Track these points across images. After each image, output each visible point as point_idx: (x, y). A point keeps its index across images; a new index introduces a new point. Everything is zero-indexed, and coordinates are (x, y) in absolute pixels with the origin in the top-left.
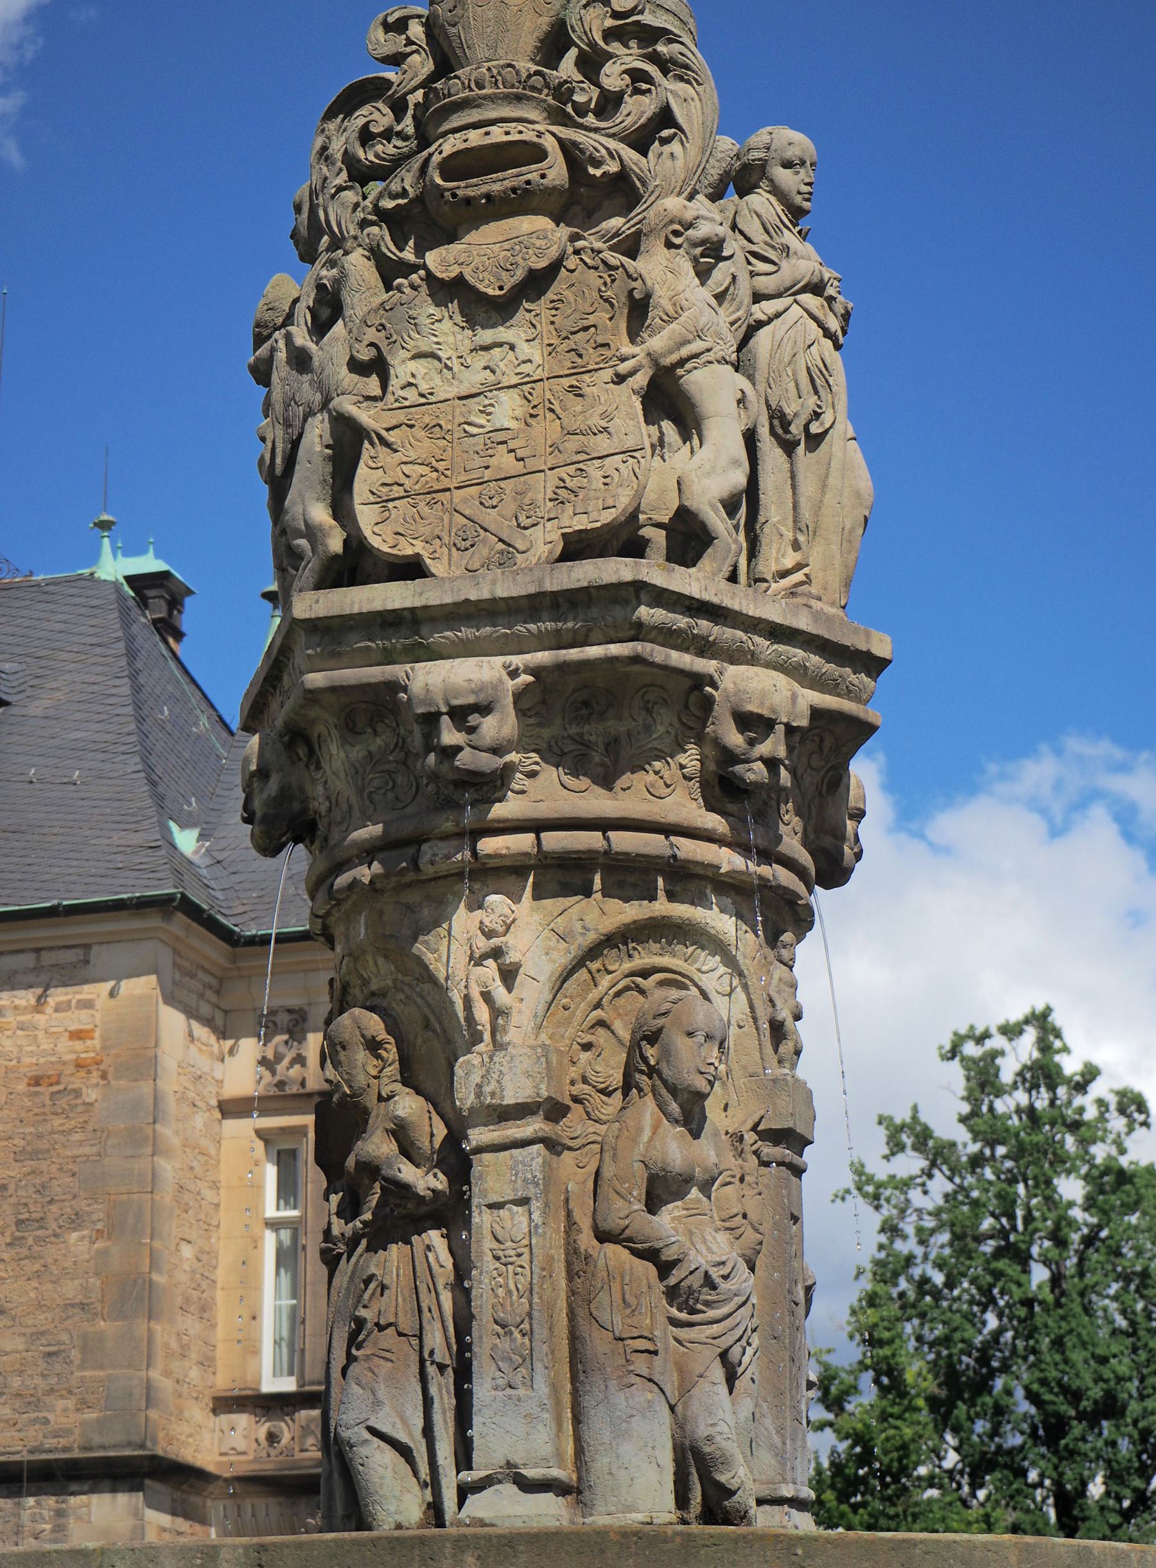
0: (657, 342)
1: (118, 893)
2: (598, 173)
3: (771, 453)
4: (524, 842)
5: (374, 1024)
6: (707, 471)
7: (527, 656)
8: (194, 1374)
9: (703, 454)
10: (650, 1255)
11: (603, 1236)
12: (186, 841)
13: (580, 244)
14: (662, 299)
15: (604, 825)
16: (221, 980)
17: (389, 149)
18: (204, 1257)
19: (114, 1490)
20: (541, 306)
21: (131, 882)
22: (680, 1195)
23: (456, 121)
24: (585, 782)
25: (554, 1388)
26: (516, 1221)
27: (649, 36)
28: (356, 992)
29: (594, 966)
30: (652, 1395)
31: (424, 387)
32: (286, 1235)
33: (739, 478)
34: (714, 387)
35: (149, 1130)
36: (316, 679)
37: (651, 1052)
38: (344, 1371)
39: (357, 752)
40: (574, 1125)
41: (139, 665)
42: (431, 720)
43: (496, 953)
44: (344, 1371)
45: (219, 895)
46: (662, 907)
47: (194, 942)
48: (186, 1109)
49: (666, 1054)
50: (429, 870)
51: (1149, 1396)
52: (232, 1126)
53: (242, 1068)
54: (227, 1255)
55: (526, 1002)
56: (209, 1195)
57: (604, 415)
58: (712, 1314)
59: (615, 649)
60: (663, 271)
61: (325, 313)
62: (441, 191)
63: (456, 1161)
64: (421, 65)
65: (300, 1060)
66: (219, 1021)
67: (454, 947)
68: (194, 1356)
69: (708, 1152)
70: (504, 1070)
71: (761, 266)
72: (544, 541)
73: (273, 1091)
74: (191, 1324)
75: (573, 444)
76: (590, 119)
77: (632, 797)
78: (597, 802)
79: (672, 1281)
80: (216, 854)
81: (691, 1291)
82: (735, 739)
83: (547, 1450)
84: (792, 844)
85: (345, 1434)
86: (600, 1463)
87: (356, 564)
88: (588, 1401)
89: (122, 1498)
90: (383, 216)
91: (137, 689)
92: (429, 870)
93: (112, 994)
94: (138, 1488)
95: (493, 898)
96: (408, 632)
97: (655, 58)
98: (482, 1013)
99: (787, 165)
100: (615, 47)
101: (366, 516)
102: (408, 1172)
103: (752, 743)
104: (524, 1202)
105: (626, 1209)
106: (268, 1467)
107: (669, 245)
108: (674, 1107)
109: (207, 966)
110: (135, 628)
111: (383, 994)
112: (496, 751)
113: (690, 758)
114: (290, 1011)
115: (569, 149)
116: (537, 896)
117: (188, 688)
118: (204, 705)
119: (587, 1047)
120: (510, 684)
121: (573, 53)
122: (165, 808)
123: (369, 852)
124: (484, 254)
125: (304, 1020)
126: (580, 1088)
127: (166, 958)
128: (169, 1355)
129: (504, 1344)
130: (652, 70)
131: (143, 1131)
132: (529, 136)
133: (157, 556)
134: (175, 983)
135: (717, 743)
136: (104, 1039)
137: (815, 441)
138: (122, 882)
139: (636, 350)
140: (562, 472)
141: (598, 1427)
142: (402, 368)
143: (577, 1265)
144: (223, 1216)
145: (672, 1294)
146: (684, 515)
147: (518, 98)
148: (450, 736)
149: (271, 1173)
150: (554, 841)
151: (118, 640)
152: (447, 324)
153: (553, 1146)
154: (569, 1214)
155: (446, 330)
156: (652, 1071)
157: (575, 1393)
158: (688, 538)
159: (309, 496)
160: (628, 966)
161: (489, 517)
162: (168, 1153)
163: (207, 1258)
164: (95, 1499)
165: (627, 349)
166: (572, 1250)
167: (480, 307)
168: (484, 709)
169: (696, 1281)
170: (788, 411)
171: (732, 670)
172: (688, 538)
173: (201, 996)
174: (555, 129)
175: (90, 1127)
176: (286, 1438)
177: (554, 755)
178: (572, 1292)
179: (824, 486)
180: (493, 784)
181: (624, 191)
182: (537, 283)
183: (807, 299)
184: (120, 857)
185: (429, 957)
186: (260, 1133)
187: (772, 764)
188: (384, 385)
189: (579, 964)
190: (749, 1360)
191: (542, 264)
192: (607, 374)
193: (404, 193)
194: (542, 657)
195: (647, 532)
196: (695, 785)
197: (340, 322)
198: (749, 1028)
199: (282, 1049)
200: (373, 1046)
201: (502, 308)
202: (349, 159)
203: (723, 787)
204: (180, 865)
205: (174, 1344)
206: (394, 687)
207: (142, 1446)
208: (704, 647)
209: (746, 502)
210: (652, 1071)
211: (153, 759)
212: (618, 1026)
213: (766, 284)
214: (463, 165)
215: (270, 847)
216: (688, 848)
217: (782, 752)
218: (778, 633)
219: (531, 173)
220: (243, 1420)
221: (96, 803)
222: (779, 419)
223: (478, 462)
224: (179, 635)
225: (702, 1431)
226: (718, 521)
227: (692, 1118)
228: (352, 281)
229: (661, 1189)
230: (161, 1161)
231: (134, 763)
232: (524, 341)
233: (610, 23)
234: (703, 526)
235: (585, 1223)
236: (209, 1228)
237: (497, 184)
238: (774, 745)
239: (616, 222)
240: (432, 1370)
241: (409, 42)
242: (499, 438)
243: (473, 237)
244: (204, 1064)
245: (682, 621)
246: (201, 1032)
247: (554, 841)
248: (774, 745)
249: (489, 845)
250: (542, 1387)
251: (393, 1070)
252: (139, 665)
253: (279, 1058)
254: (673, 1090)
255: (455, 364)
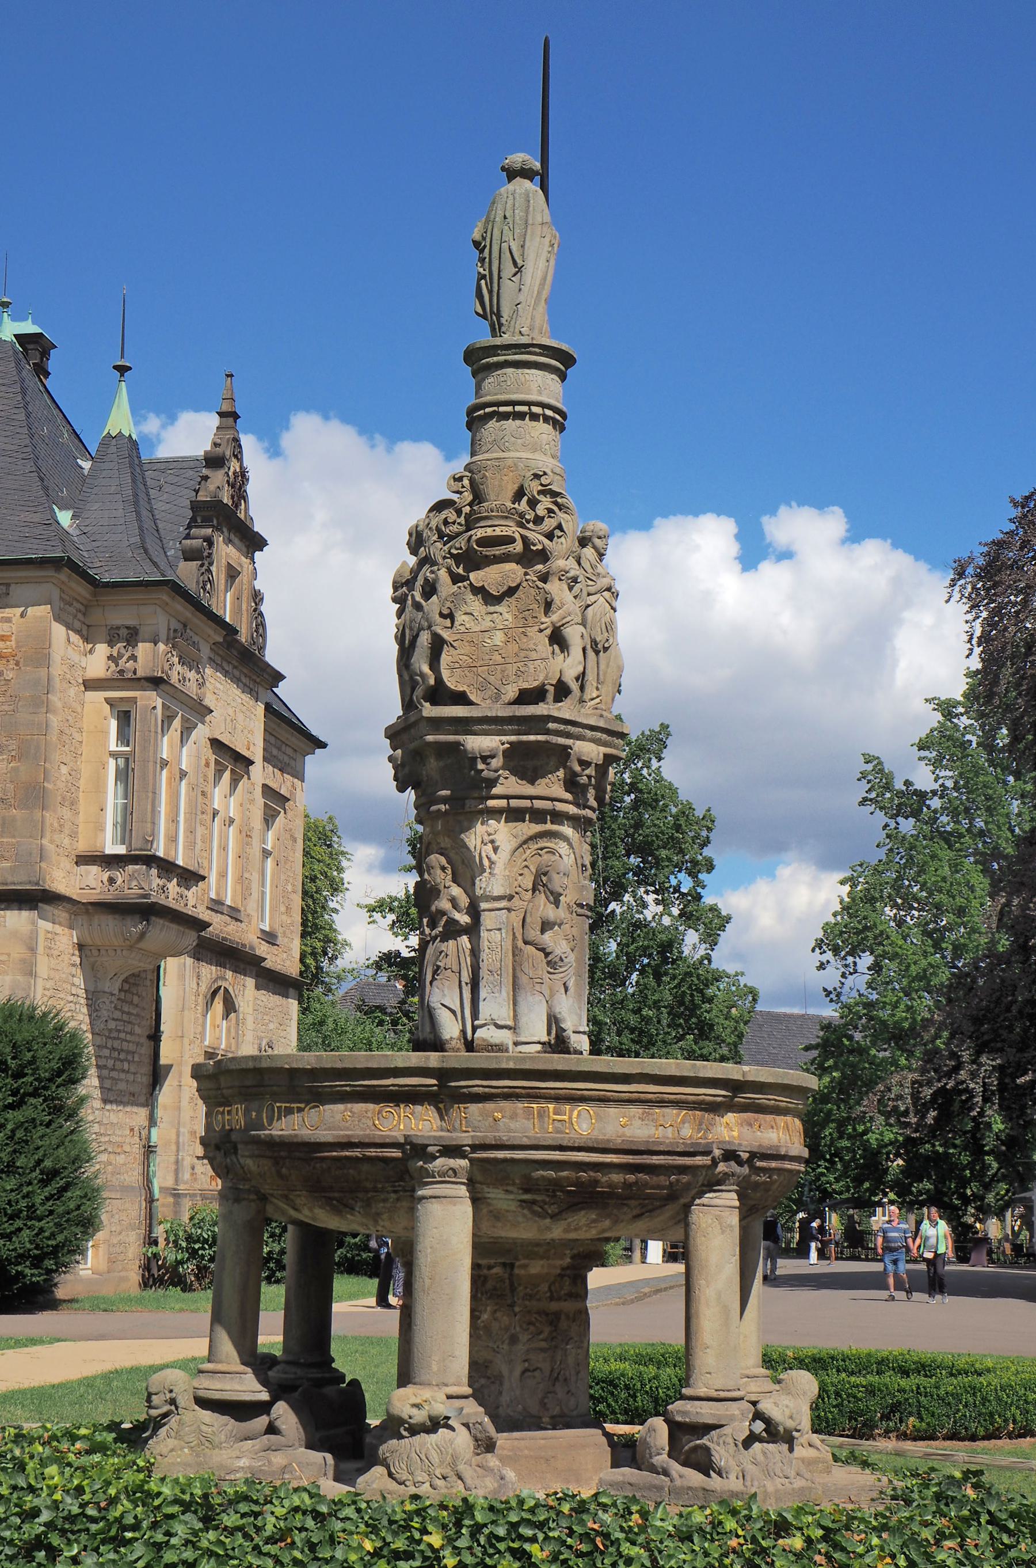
0: (555, 617)
1: (28, 554)
2: (534, 548)
3: (591, 654)
4: (503, 803)
5: (443, 861)
6: (570, 666)
7: (508, 737)
8: (67, 841)
9: (569, 660)
10: (543, 950)
11: (526, 943)
12: (65, 518)
13: (528, 577)
14: (557, 601)
15: (531, 798)
16: (86, 607)
17: (455, 528)
18: (73, 773)
19: (20, 909)
20: (512, 600)
21: (36, 547)
22: (551, 929)
23: (482, 524)
24: (524, 782)
25: (508, 994)
26: (496, 936)
27: (555, 494)
28: (434, 846)
29: (525, 846)
30: (541, 998)
31: (468, 626)
32: (121, 762)
33: (581, 669)
34: (574, 634)
35: (44, 697)
36: (430, 738)
37: (544, 879)
38: (431, 983)
39: (441, 764)
40: (516, 902)
41: (28, 399)
42: (474, 760)
43: (492, 842)
44: (431, 983)
45: (85, 554)
46: (549, 826)
47: (73, 585)
48: (66, 685)
49: (550, 880)
50: (467, 809)
51: (610, 858)
52: (90, 695)
53: (97, 661)
54: (86, 771)
55: (501, 859)
56: (77, 736)
57: (534, 644)
58: (561, 970)
59: (540, 738)
60: (556, 588)
61: (428, 589)
62: (477, 551)
63: (474, 911)
64: (468, 497)
65: (133, 658)
66: (85, 633)
67: (475, 837)
68: (67, 831)
69: (562, 913)
70: (493, 883)
71: (590, 583)
72: (511, 692)
73: (116, 676)
74: (66, 813)
75: (522, 654)
76: (531, 525)
77: (541, 787)
78: (529, 790)
79: (549, 959)
80: (82, 528)
81: (556, 963)
82: (577, 768)
83: (505, 1015)
84: (593, 803)
85: (432, 1005)
86: (523, 1020)
87: (439, 694)
88: (519, 999)
89: (25, 914)
90: (452, 556)
91: (28, 415)
92: (467, 809)
93: (22, 615)
94: (34, 908)
95: (490, 822)
96: (465, 725)
97: (556, 503)
98: (486, 862)
99: (599, 538)
100: (541, 498)
101: (445, 674)
102: (457, 916)
103: (583, 770)
104: (499, 929)
105: (534, 934)
106: (109, 897)
107: (560, 580)
108: (551, 898)
109: (79, 598)
110: (24, 373)
111: (446, 849)
112: (496, 771)
113: (561, 773)
114: (128, 628)
115: (524, 538)
116: (506, 822)
117: (56, 412)
118: (64, 423)
119: (521, 875)
120: (502, 747)
121: (525, 498)
122: (50, 498)
123: (444, 800)
124: (489, 577)
125: (137, 634)
126: (518, 889)
127: (56, 594)
128: (53, 831)
129: (491, 978)
130: (555, 508)
131: (40, 699)
132: (509, 533)
133: (34, 323)
134: (60, 609)
135: (571, 769)
136: (17, 642)
137: (606, 649)
138: (30, 546)
139: (547, 620)
140: (519, 664)
141: (522, 1008)
142: (460, 618)
143: (516, 952)
144: (85, 749)
145: (549, 963)
146: (560, 681)
147: (507, 517)
148: (481, 766)
149: (114, 724)
150: (514, 803)
151: (15, 382)
152: (477, 603)
153: (509, 910)
154: (514, 934)
155: (475, 604)
156: (544, 885)
157: (514, 996)
158: (562, 691)
159: (422, 661)
160: (536, 846)
161: (492, 679)
162: (55, 712)
163: (74, 773)
164: (8, 913)
165: (544, 619)
166: (515, 947)
167: (490, 599)
168: (493, 757)
169: (557, 959)
170: (598, 640)
171: (578, 742)
172: (562, 691)
173: (75, 616)
174: (519, 529)
175: (8, 694)
176: (119, 881)
177: (514, 773)
178: (514, 961)
179: (608, 666)
180: (492, 783)
181: (543, 556)
182: (511, 591)
183: (606, 594)
184: (27, 529)
185: (466, 840)
186: (107, 700)
187: (589, 777)
188: (453, 623)
189: (521, 846)
190: (571, 984)
191: (514, 585)
192: (536, 628)
193: (461, 548)
194: (513, 738)
195: (547, 687)
196: (562, 782)
197: (435, 596)
198: (575, 867)
199: (123, 651)
200: (443, 869)
201: (497, 600)
202: (438, 529)
203: (571, 783)
204: (63, 535)
205: (56, 825)
206: (458, 744)
207: (37, 884)
208: (568, 735)
209: (581, 678)
210: (544, 885)
211: (40, 462)
212: (531, 867)
213: (592, 589)
214: (484, 542)
215: (401, 789)
216: (560, 807)
217: (593, 774)
218: (593, 728)
219: (510, 548)
220: (94, 869)
221: (8, 492)
222: (594, 643)
223: (488, 657)
224: (47, 374)
225: (557, 1010)
226: (574, 686)
227: (557, 903)
228: (441, 581)
229: (546, 926)
230: (50, 716)
231: (30, 466)
232: (506, 612)
233: (540, 488)
234: (568, 687)
235: (519, 937)
236: (77, 755)
237: (498, 551)
238: (591, 771)
239: (540, 567)
240: (463, 984)
241: (463, 487)
242: (495, 649)
243: (487, 569)
244: (76, 657)
245: (562, 727)
246: (75, 638)
247: (514, 803)
248: (591, 771)
249: (491, 803)
250: (504, 993)
251: (450, 877)
252: (28, 399)
253: (120, 656)
254: (552, 893)
255: (479, 618)
